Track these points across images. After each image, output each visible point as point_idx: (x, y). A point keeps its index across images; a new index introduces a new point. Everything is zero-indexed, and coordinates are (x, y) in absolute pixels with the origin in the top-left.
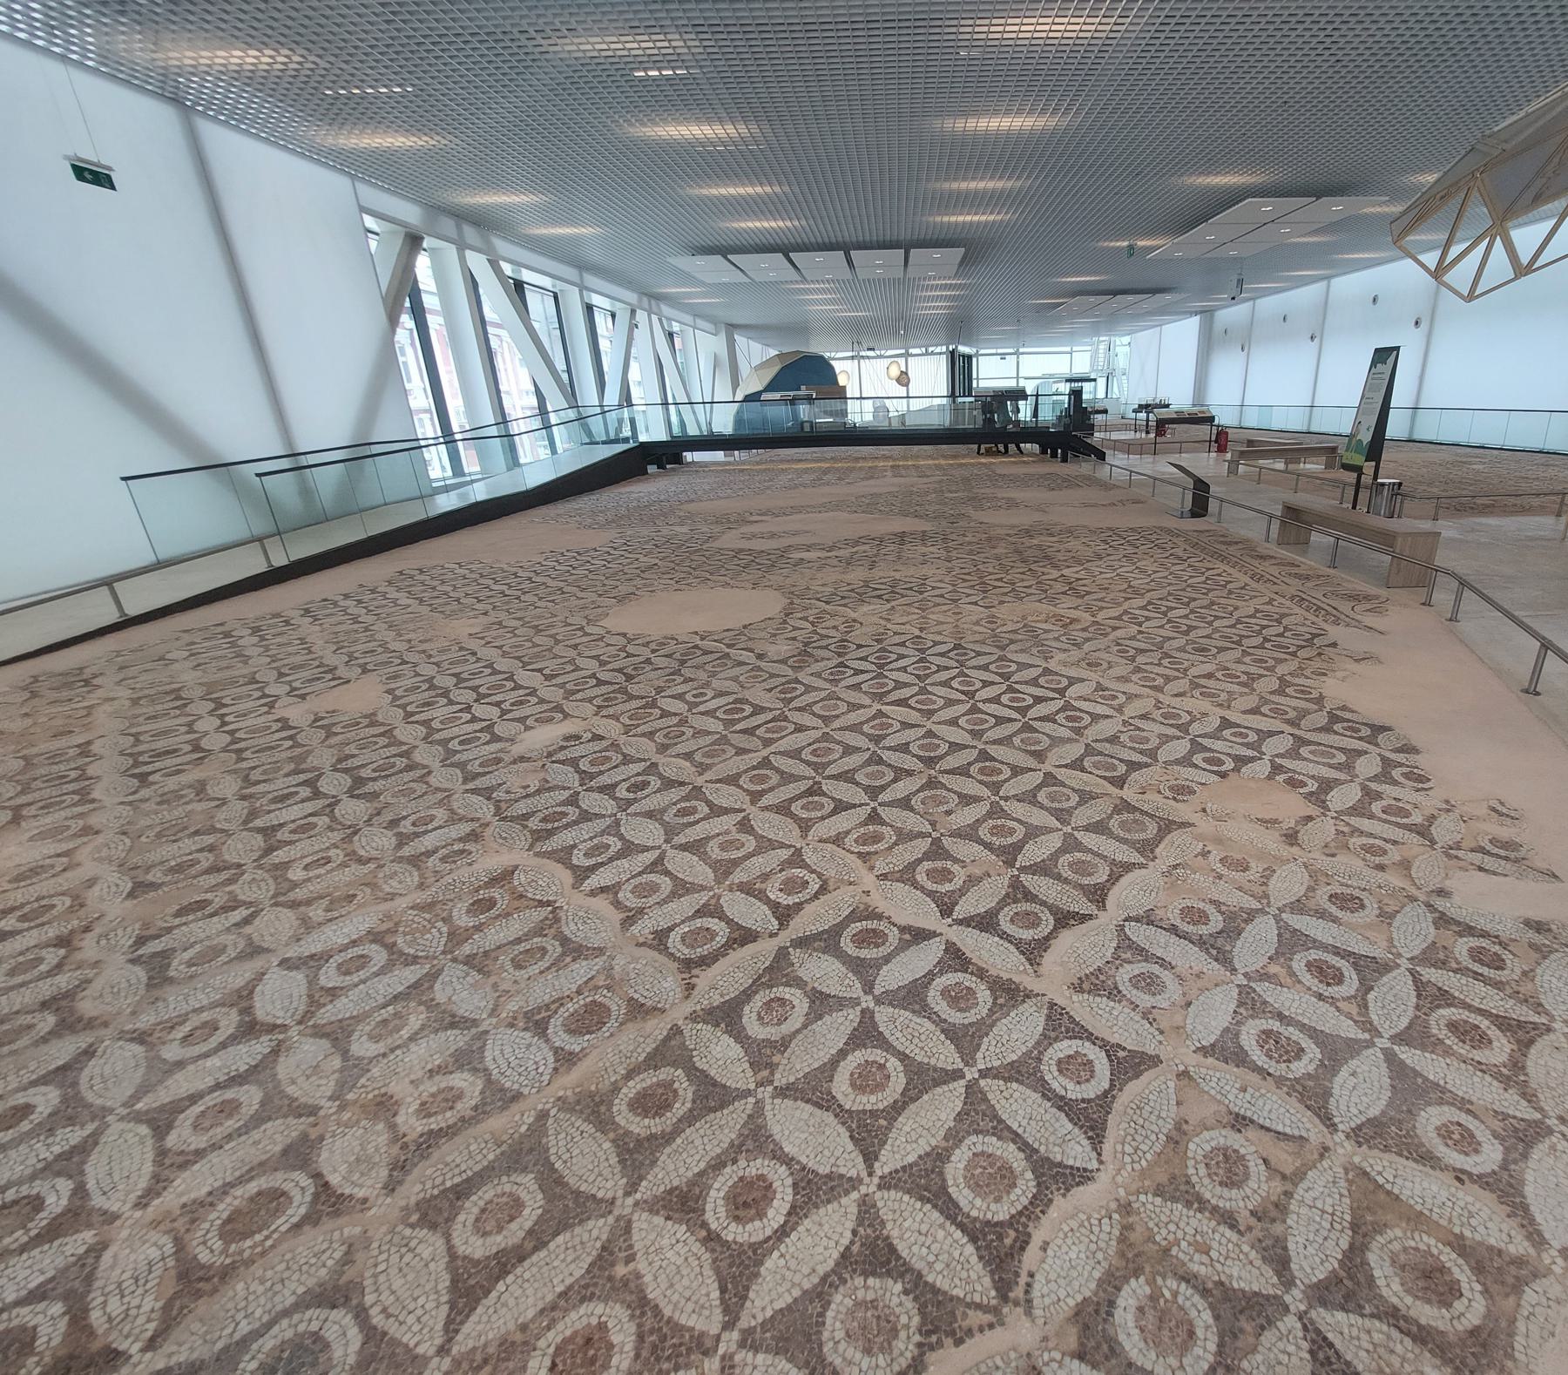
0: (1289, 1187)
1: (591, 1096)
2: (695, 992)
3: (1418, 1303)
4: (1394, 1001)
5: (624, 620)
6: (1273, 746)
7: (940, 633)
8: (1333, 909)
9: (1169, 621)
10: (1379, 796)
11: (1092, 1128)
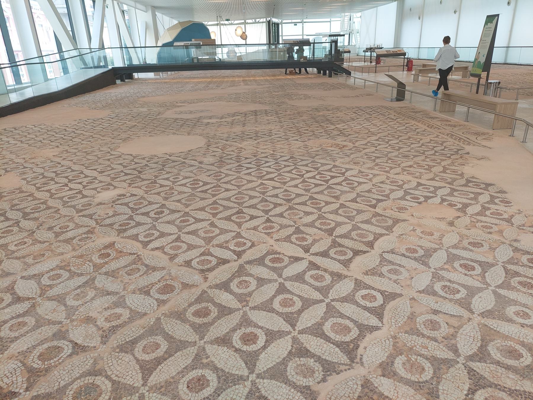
0: (457, 330)
1: (176, 312)
2: (209, 280)
3: (507, 359)
4: (496, 276)
5: (126, 149)
6: (440, 192)
7: (283, 152)
8: (470, 247)
9: (390, 145)
10: (489, 209)
11: (378, 315)
